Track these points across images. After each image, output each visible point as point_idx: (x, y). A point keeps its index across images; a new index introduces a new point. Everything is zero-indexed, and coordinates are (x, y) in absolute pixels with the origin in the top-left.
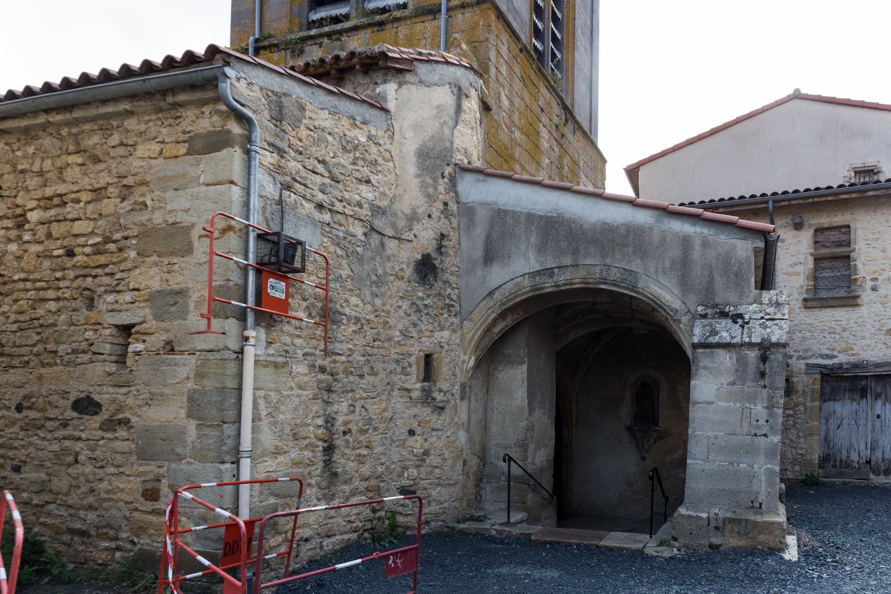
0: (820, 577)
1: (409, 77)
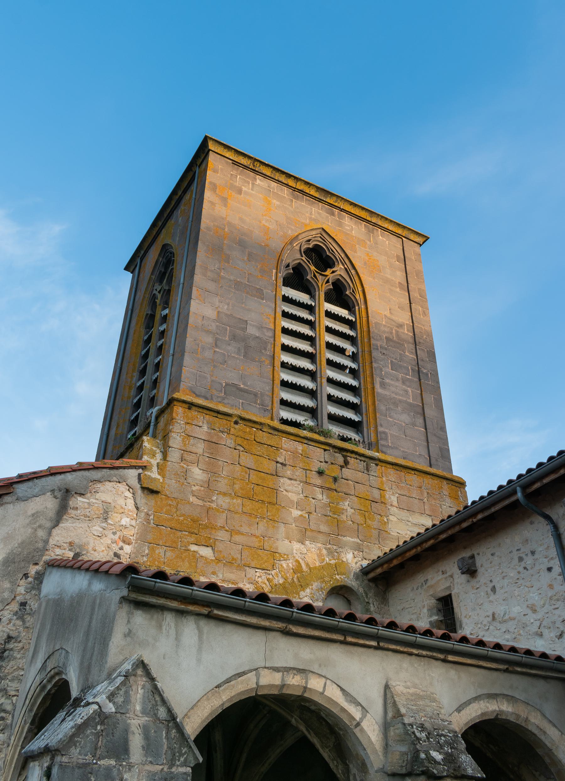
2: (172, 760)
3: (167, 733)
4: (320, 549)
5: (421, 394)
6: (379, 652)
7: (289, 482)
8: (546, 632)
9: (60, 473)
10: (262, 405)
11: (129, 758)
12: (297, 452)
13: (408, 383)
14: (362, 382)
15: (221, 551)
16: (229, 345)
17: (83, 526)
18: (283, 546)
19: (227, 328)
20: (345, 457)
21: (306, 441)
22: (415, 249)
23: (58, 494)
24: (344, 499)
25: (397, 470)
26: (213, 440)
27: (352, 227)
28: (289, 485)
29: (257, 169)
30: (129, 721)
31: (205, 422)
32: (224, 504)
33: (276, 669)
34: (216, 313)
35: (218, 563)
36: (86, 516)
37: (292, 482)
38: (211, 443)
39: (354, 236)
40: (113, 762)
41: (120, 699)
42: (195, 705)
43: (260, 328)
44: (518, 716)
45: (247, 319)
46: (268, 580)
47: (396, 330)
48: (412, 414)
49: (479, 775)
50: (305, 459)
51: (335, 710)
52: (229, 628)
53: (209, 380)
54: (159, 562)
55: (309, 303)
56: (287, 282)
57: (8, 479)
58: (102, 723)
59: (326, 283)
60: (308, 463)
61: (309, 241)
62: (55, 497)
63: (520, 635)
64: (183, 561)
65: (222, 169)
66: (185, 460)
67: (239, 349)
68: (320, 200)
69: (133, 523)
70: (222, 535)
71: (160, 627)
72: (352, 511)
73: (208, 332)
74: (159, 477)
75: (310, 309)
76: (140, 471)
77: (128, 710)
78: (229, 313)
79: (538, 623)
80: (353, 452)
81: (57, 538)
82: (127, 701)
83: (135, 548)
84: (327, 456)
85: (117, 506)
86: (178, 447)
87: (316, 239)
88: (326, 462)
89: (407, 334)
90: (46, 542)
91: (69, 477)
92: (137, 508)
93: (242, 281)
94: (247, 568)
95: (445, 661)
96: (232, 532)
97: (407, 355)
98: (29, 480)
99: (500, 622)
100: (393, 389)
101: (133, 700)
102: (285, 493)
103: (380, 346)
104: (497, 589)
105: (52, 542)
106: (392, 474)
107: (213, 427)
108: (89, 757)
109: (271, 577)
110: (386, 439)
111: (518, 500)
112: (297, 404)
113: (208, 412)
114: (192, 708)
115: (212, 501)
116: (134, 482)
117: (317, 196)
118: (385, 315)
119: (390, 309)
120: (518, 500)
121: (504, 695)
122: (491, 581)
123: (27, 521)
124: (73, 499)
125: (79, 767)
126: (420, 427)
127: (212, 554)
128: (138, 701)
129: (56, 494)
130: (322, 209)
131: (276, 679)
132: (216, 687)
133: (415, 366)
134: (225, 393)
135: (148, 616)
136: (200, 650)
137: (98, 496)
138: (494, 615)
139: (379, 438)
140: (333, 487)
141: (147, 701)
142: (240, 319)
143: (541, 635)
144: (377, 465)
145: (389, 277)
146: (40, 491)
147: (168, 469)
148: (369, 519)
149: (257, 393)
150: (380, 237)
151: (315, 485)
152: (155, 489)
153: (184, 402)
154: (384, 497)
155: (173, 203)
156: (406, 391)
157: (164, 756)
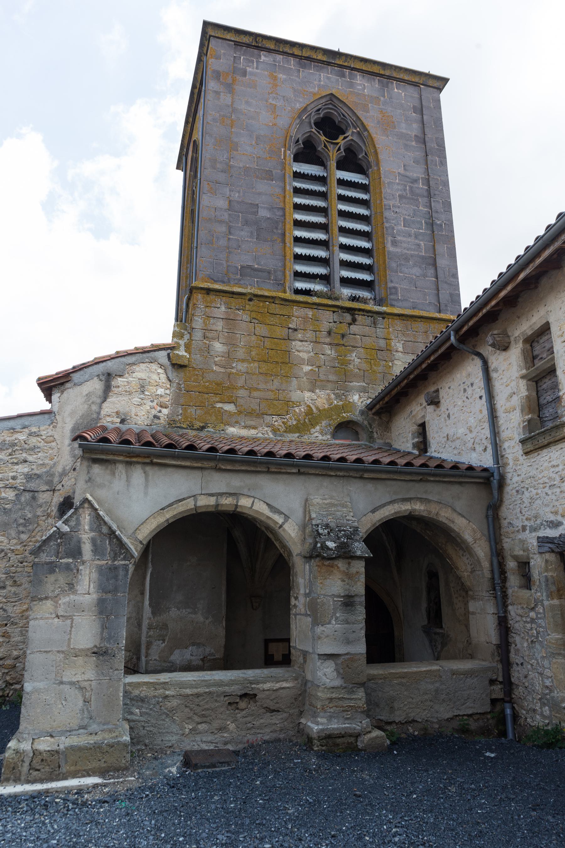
0: (25, 836)
1: (68, 385)
2: (114, 557)
3: (110, 542)
4: (328, 395)
5: (434, 246)
6: (302, 477)
7: (300, 343)
8: (477, 447)
9: (102, 362)
10: (276, 280)
11: (82, 557)
12: (308, 317)
13: (420, 237)
14: (374, 243)
15: (242, 405)
16: (242, 230)
17: (125, 399)
18: (296, 395)
19: (239, 215)
20: (353, 315)
21: (315, 307)
22: (434, 95)
23: (103, 378)
24: (352, 351)
25: (404, 320)
26: (231, 318)
27: (364, 85)
28: (300, 346)
29: (260, 45)
30: (80, 536)
31: (222, 303)
32: (242, 369)
33: (212, 495)
34: (227, 203)
35: (239, 414)
36: (126, 391)
37: (303, 343)
38: (229, 320)
39: (366, 95)
40: (71, 560)
41: (73, 523)
42: (144, 522)
43: (271, 209)
44: (430, 512)
45: (257, 203)
46: (283, 423)
47: (410, 186)
48: (424, 266)
49: (366, 555)
50: (316, 322)
51: (263, 519)
52: (170, 470)
53: (225, 265)
54: (191, 419)
55: (321, 175)
56: (298, 158)
57: (66, 371)
58: (61, 538)
59: (337, 151)
60: (317, 326)
61: (319, 110)
62: (101, 380)
63: (462, 450)
64: (211, 415)
65: (224, 54)
66: (207, 337)
67: (252, 233)
68: (329, 64)
69: (168, 392)
70: (242, 393)
71: (113, 474)
72: (359, 360)
73: (221, 222)
74: (185, 354)
75: (322, 180)
76: (169, 351)
77: (79, 529)
78: (240, 200)
79: (472, 441)
80: (360, 310)
81: (106, 410)
82: (78, 523)
83: (171, 410)
84: (336, 317)
85: (151, 381)
86: (200, 327)
87: (326, 107)
88: (335, 322)
89: (422, 188)
90: (99, 413)
91: (109, 363)
92: (170, 381)
93: (251, 166)
94: (265, 416)
95: (361, 478)
96: (251, 389)
97: (421, 210)
98: (80, 369)
99: (452, 442)
100: (405, 245)
101: (82, 523)
102: (296, 353)
103: (393, 205)
104: (451, 416)
105: (103, 413)
106: (399, 324)
107: (229, 307)
108: (53, 558)
109: (285, 420)
110: (396, 293)
111: (452, 345)
112: (311, 273)
113: (224, 294)
114: (142, 524)
115: (233, 368)
116: (165, 361)
117: (325, 59)
118: (399, 173)
119: (404, 166)
120: (452, 345)
121: (418, 498)
122: (447, 409)
123: (83, 400)
124: (115, 380)
125: (47, 564)
126: (432, 277)
127: (235, 409)
128: (87, 523)
129: (101, 378)
130: (331, 72)
131: (212, 501)
132: (161, 510)
133: (430, 219)
134: (240, 275)
135: (104, 468)
136: (146, 486)
137: (134, 375)
138: (447, 435)
139: (388, 293)
140: (342, 342)
141: (93, 523)
142: (252, 204)
143: (474, 449)
144: (384, 318)
145: (404, 131)
146: (90, 376)
147: (193, 346)
148: (375, 365)
149: (270, 270)
150: (396, 90)
151: (324, 343)
152: (182, 364)
153: (202, 289)
154: (390, 345)
155: (195, 97)
156: (419, 245)
157: (108, 555)
